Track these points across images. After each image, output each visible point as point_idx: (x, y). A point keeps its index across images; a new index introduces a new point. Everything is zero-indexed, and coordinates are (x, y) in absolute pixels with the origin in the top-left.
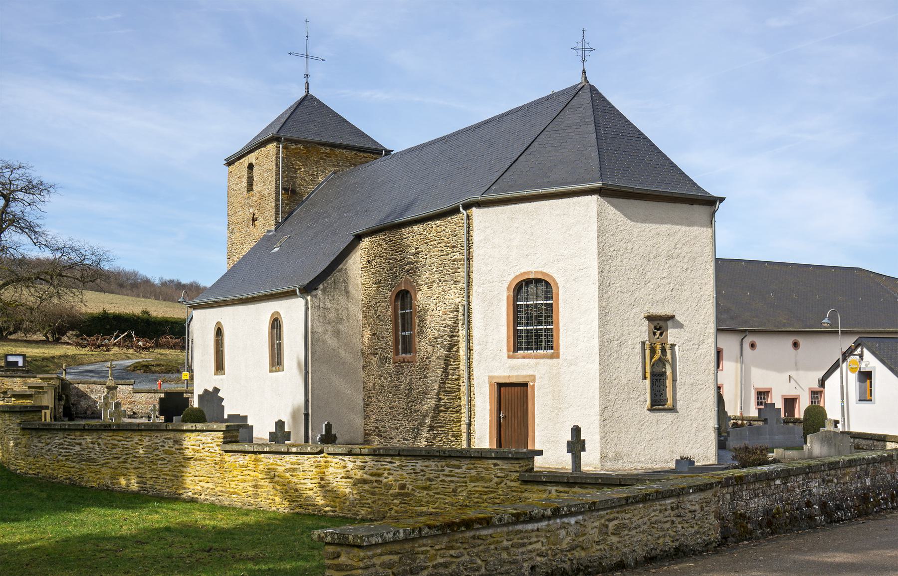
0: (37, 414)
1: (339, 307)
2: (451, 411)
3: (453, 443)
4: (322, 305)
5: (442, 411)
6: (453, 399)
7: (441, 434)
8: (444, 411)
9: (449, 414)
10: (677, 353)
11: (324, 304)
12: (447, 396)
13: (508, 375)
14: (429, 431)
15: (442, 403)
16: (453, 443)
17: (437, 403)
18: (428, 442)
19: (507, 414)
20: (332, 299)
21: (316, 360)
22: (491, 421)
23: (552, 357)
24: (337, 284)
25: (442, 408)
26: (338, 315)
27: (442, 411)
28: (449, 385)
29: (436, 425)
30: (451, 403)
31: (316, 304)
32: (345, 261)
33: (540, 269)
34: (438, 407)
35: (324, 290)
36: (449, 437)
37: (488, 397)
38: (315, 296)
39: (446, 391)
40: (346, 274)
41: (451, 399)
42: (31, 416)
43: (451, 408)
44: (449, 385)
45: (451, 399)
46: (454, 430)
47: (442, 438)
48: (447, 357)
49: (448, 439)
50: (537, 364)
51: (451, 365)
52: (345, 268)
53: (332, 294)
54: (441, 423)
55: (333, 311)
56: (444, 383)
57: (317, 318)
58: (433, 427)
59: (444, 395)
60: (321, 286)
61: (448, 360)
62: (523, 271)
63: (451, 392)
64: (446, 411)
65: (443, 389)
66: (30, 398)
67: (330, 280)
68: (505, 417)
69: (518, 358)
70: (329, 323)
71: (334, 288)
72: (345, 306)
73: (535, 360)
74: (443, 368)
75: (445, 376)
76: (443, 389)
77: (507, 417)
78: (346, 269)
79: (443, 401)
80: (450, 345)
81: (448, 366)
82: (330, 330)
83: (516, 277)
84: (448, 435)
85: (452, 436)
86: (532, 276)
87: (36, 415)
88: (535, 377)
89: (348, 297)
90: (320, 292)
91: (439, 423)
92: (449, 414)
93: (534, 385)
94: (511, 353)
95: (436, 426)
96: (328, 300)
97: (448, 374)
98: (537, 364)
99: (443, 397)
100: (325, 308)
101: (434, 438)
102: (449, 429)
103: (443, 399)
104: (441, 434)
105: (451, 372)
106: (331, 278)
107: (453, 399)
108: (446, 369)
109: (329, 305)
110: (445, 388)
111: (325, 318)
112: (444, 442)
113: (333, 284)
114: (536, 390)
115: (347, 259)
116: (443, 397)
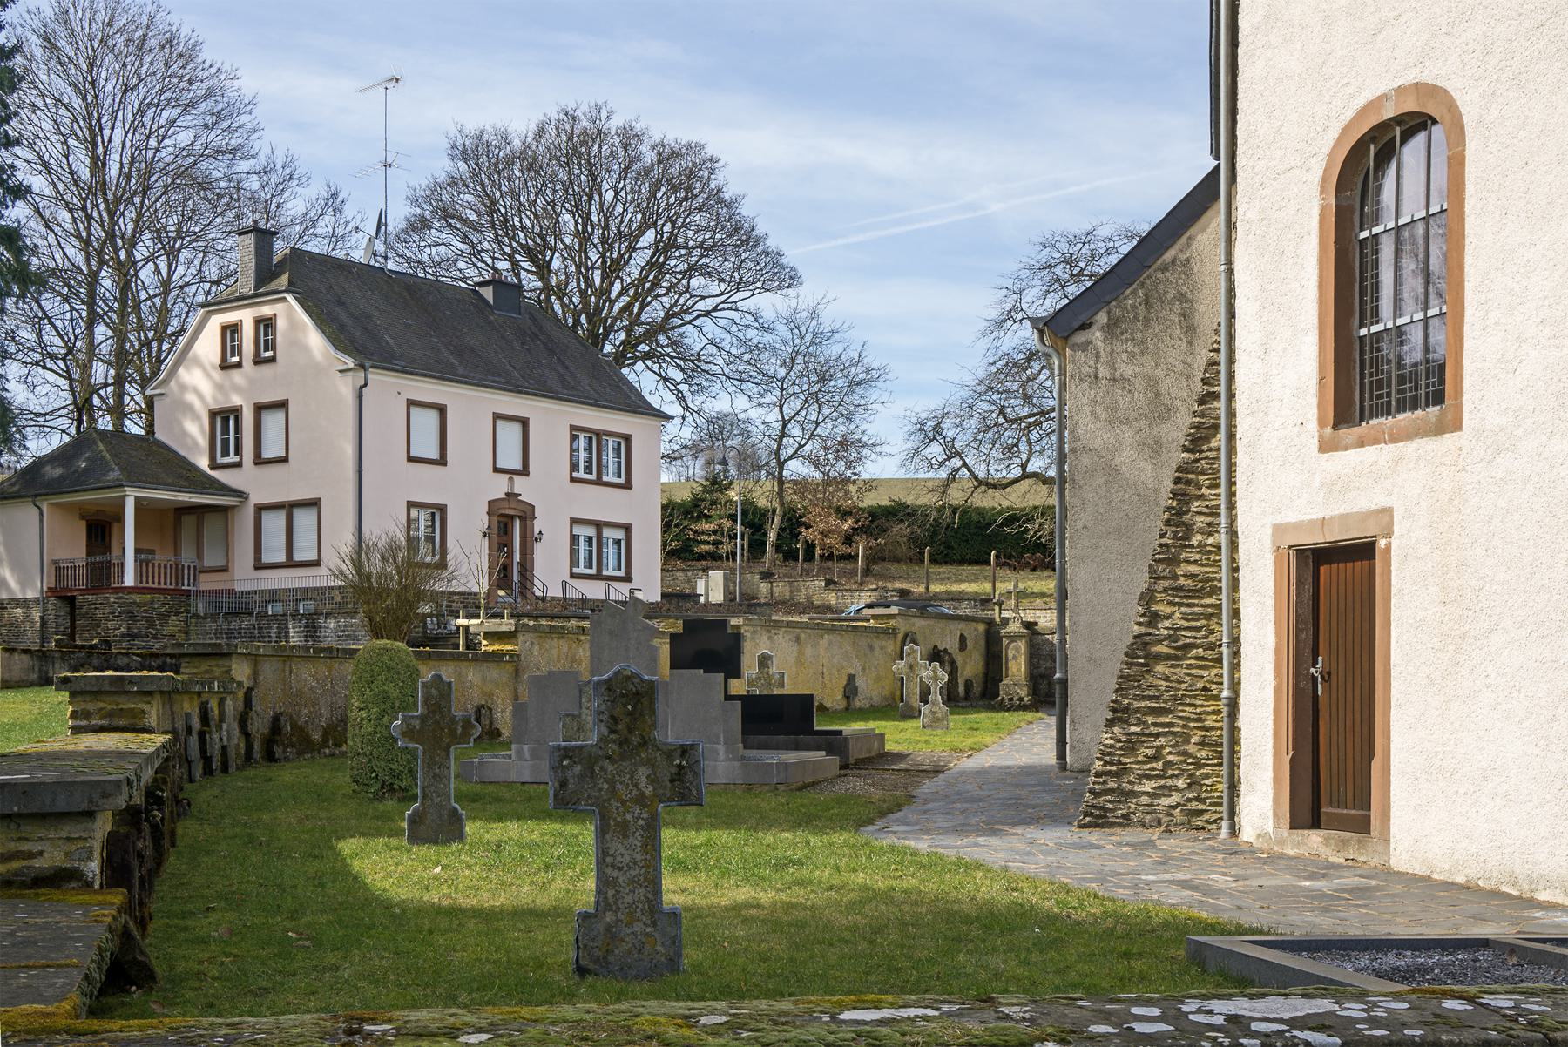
0: (220, 662)
1: (1160, 373)
2: (1197, 658)
3: (1207, 770)
4: (1103, 372)
5: (1160, 658)
6: (1209, 617)
7: (1158, 735)
8: (1168, 657)
9: (1190, 667)
10: (1223, 252)
11: (1112, 366)
12: (1180, 605)
13: (1320, 515)
14: (1110, 723)
15: (1163, 628)
16: (1207, 770)
17: (1143, 630)
18: (1106, 763)
19: (1334, 665)
20: (1137, 350)
21: (1085, 527)
22: (1277, 690)
23: (1439, 429)
24: (1157, 306)
25: (1163, 648)
26: (1157, 395)
27: (1160, 658)
28: (1193, 569)
29: (1136, 705)
30: (1198, 629)
31: (1086, 370)
32: (1184, 239)
33: (1409, 78)
34: (1146, 644)
35: (1112, 329)
36: (1191, 748)
37: (1270, 602)
38: (1084, 347)
39: (1181, 589)
40: (1188, 274)
41: (1197, 617)
42: (204, 667)
43: (1197, 646)
44: (1193, 569)
45: (1197, 617)
46: (1208, 724)
47: (1159, 749)
48: (1186, 471)
49: (1186, 754)
50: (1398, 461)
51: (1201, 497)
52: (1183, 257)
53: (1139, 336)
54: (1157, 698)
55: (1139, 384)
56: (1173, 561)
57: (1087, 409)
58: (1126, 710)
59: (1170, 603)
60: (1102, 318)
61: (1188, 482)
62: (1361, 101)
63: (1197, 593)
64: (1177, 658)
65: (1167, 583)
66: (513, 640)
67: (1132, 298)
68: (1327, 676)
69: (1346, 449)
70: (1127, 422)
71: (1147, 320)
72: (1179, 368)
73: (1392, 448)
74: (1168, 509)
75: (1175, 537)
76: (1167, 583)
77: (1334, 677)
78: (1188, 260)
79: (1167, 623)
80: (1197, 427)
81: (1188, 503)
82: (1130, 441)
83: (1345, 130)
84: (1187, 742)
85: (1202, 744)
86: (1389, 113)
87: (217, 666)
88: (1392, 517)
89: (1190, 343)
90: (1098, 334)
91: (1150, 698)
92: (1190, 667)
93: (1388, 548)
94: (1329, 430)
95: (1138, 710)
96: (1125, 356)
97: (1189, 530)
98: (1398, 461)
99: (1168, 610)
100: (1114, 380)
101: (1131, 747)
102: (1189, 719)
103: (1168, 617)
104: (1158, 735)
105: (1200, 521)
106: (1134, 292)
107: (1209, 617)
108: (1180, 513)
109: (1126, 369)
110: (1175, 577)
111: (1113, 407)
112: (1168, 764)
113: (1141, 309)
114: (1394, 558)
115: (1191, 232)
116: (1168, 610)
